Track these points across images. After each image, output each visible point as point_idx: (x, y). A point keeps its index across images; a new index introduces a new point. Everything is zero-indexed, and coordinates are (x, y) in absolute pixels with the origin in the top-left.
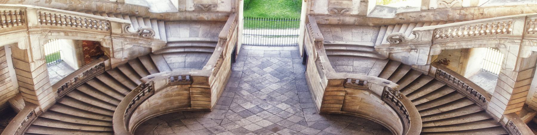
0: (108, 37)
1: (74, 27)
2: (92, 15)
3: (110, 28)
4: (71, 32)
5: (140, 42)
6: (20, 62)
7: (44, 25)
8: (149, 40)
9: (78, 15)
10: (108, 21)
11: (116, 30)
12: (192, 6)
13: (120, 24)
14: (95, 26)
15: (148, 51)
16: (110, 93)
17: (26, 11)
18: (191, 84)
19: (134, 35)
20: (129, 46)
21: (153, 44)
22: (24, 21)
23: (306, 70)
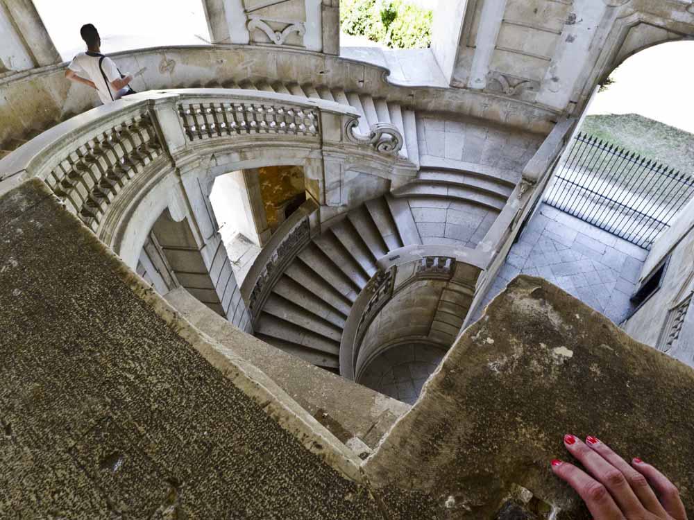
0: (316, 154)
1: (253, 132)
2: (269, 93)
3: (319, 129)
4: (250, 147)
5: (374, 164)
6: (181, 254)
7: (196, 139)
8: (389, 160)
9: (258, 99)
10: (318, 109)
11: (331, 135)
12: (482, 78)
13: (338, 116)
14: (292, 125)
15: (382, 188)
16: (326, 296)
17: (154, 113)
18: (448, 281)
19: (362, 145)
20: (352, 175)
21: (395, 172)
22: (157, 141)
23: (628, 319)
